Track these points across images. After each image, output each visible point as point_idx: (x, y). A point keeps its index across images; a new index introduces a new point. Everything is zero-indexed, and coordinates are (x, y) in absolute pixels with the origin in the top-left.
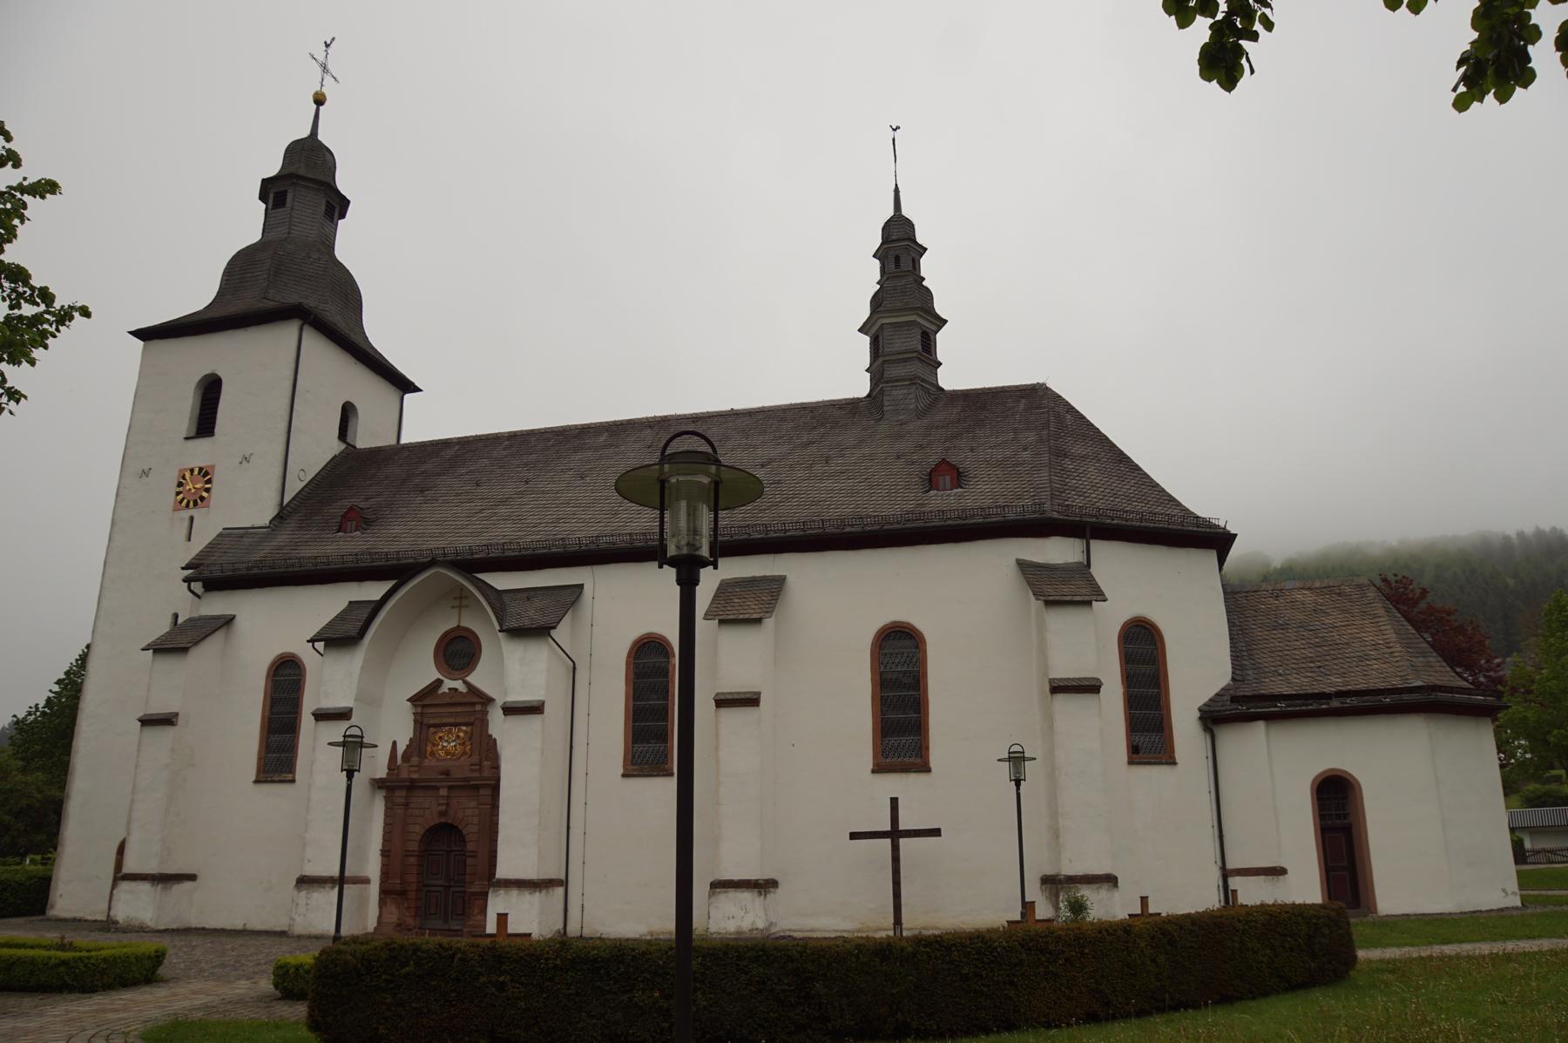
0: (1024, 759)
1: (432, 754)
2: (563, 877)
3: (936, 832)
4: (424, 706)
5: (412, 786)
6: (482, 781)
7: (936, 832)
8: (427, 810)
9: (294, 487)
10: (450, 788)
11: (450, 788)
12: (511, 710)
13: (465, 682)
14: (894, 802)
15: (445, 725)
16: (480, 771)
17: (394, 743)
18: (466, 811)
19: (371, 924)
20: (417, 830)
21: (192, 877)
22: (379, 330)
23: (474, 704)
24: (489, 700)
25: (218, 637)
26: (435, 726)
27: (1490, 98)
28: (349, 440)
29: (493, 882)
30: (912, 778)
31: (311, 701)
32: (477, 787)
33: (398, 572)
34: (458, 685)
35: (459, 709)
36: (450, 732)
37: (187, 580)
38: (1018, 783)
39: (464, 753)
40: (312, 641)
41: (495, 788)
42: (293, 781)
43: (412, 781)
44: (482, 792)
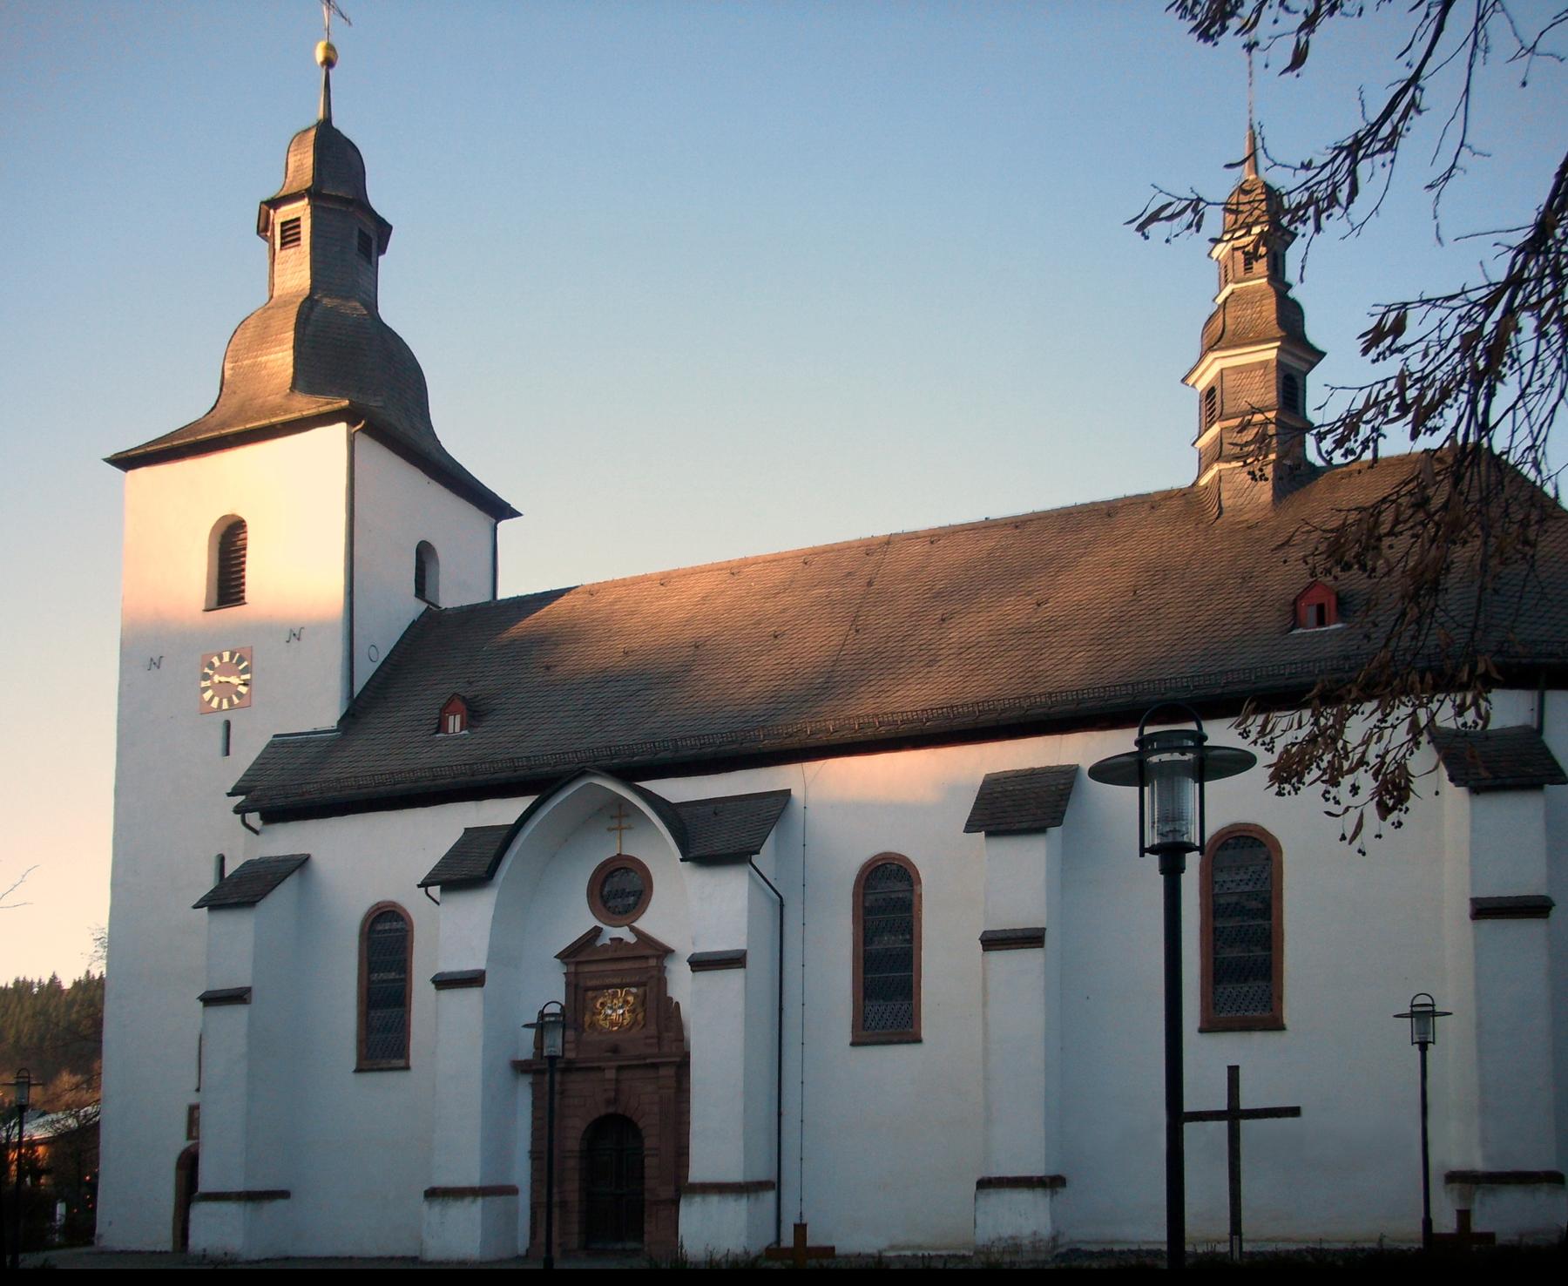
0: (1434, 1014)
1: (593, 1025)
2: (774, 1178)
3: (1294, 1112)
4: (578, 963)
6: (664, 1051)
7: (1294, 1112)
8: (586, 1101)
9: (365, 671)
10: (620, 1068)
12: (701, 963)
13: (633, 929)
14: (1233, 1071)
18: (643, 1096)
19: (522, 1243)
21: (284, 1194)
22: (455, 427)
23: (646, 958)
24: (666, 952)
25: (291, 883)
26: (595, 989)
27: (67, 985)
28: (428, 595)
29: (683, 1188)
30: (1257, 1038)
31: (425, 964)
32: (655, 1066)
33: (540, 783)
34: (624, 933)
36: (615, 995)
37: (240, 810)
38: (1423, 1047)
39: (634, 1023)
40: (424, 885)
41: (683, 1065)
42: (407, 1068)
43: (570, 1062)
44: (663, 1072)
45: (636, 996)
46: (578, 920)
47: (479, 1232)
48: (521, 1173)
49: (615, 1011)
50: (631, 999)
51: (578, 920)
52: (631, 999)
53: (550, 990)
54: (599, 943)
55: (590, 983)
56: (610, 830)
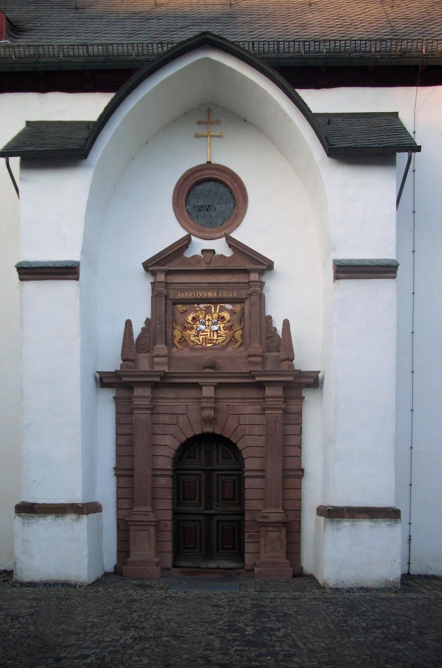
1: (183, 340)
4: (168, 273)
5: (162, 383)
8: (181, 417)
10: (219, 386)
11: (219, 386)
15: (200, 301)
16: (263, 364)
17: (129, 324)
18: (244, 420)
20: (168, 444)
23: (246, 272)
32: (261, 386)
34: (220, 246)
35: (223, 279)
36: (208, 311)
39: (232, 340)
44: (269, 392)
45: (232, 313)
46: (165, 230)
47: (85, 552)
48: (106, 492)
49: (209, 328)
50: (227, 315)
51: (165, 230)
52: (227, 315)
53: (136, 305)
54: (189, 254)
55: (181, 296)
56: (197, 136)
